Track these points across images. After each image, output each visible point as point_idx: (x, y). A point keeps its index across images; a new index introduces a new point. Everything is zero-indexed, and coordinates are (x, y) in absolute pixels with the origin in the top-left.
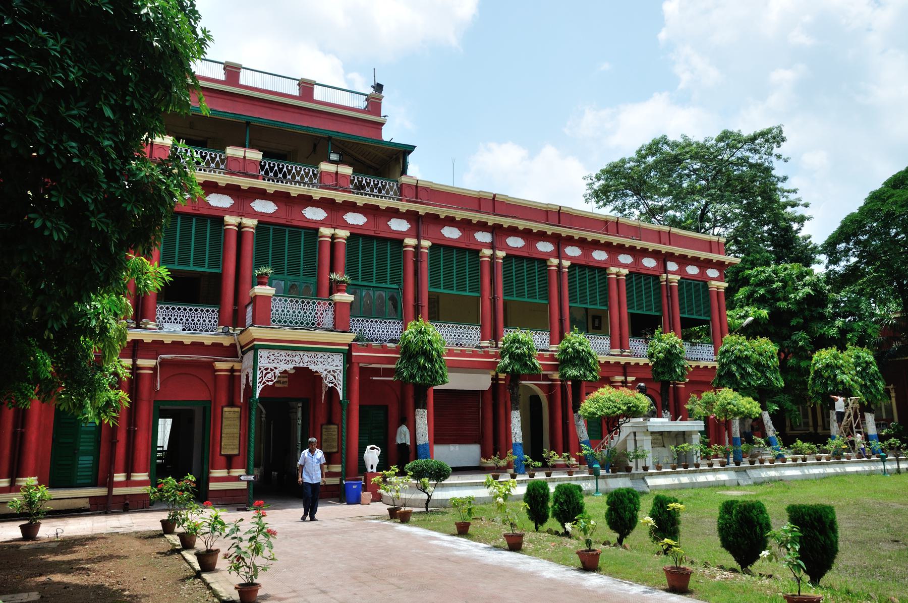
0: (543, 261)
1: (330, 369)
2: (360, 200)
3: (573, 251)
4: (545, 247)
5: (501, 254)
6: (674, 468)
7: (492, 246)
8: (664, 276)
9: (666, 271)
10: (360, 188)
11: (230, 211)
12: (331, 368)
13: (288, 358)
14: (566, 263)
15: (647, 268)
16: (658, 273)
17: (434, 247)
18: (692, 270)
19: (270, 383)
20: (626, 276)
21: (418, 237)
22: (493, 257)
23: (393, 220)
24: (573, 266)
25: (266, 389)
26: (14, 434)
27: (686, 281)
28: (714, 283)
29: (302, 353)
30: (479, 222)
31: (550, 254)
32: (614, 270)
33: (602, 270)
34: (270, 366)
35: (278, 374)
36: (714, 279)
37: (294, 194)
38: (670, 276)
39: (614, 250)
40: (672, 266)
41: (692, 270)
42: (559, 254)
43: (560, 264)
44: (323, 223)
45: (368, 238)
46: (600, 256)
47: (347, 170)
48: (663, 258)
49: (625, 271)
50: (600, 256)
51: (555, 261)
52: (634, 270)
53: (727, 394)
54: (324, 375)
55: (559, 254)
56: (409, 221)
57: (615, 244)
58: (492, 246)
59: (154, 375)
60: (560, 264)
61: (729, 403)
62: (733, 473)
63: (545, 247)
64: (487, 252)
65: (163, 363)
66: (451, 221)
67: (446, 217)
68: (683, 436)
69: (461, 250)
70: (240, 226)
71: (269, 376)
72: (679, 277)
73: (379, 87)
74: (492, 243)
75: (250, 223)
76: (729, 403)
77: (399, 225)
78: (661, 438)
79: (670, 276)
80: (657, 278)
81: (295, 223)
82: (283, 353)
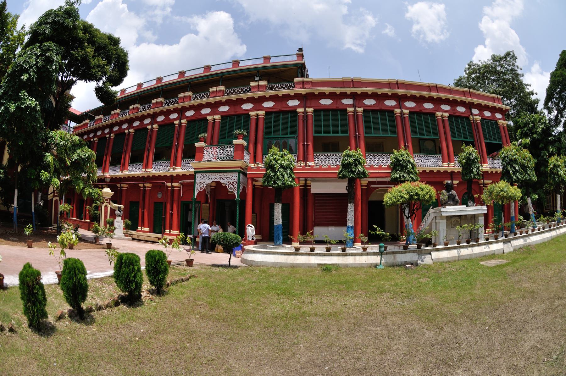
0: (391, 111)
1: (230, 181)
2: (267, 93)
3: (410, 104)
4: (390, 103)
5: (360, 110)
6: (468, 242)
7: (353, 106)
8: (471, 117)
9: (472, 114)
10: (272, 88)
11: (251, 110)
12: (231, 181)
13: (210, 177)
14: (406, 111)
15: (460, 112)
16: (467, 116)
17: (315, 111)
18: (487, 114)
19: (201, 190)
20: (448, 117)
21: (305, 107)
22: (355, 112)
23: (290, 101)
24: (411, 113)
25: (200, 192)
26: (378, 184)
27: (484, 119)
28: (500, 121)
29: (216, 174)
30: (341, 93)
31: (395, 107)
32: (439, 114)
33: (433, 115)
34: (201, 181)
35: (205, 185)
36: (500, 119)
37: (234, 99)
38: (475, 117)
39: (438, 102)
40: (475, 111)
41: (487, 114)
42: (400, 106)
43: (402, 111)
44: (251, 110)
45: (277, 113)
46: (428, 106)
47: (264, 83)
48: (469, 106)
49: (447, 115)
50: (428, 106)
51: (398, 111)
52: (452, 114)
53: (503, 184)
54: (227, 185)
55: (400, 106)
56: (299, 100)
57: (435, 98)
58: (353, 106)
59: (179, 191)
60: (402, 111)
61: (502, 191)
62: (502, 244)
63: (390, 103)
64: (350, 109)
65: (181, 184)
66: (323, 95)
67: (319, 93)
68: (474, 218)
69: (335, 111)
70: (257, 115)
71: (201, 186)
72: (480, 118)
73: (300, 50)
74: (353, 104)
75: (262, 113)
76: (502, 191)
77: (293, 103)
78: (454, 221)
79: (475, 117)
80: (468, 118)
81: (238, 113)
82: (207, 174)
